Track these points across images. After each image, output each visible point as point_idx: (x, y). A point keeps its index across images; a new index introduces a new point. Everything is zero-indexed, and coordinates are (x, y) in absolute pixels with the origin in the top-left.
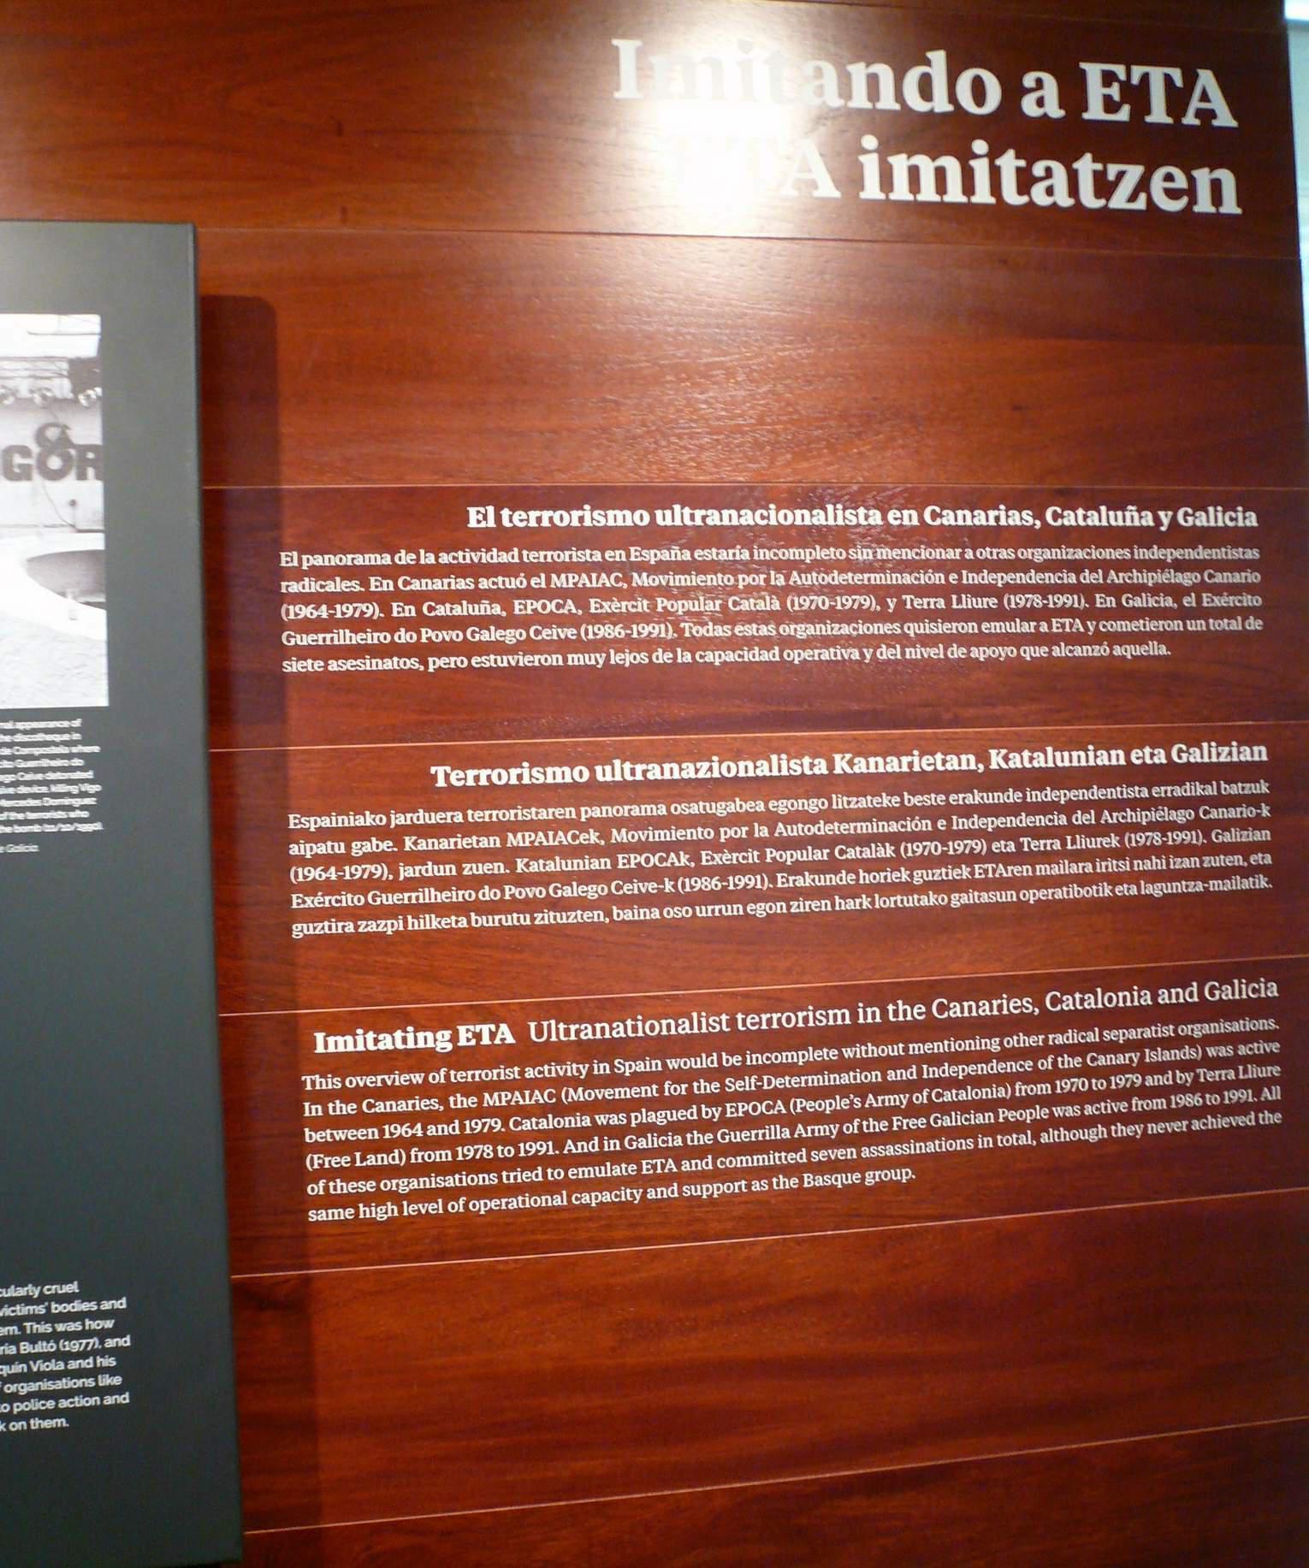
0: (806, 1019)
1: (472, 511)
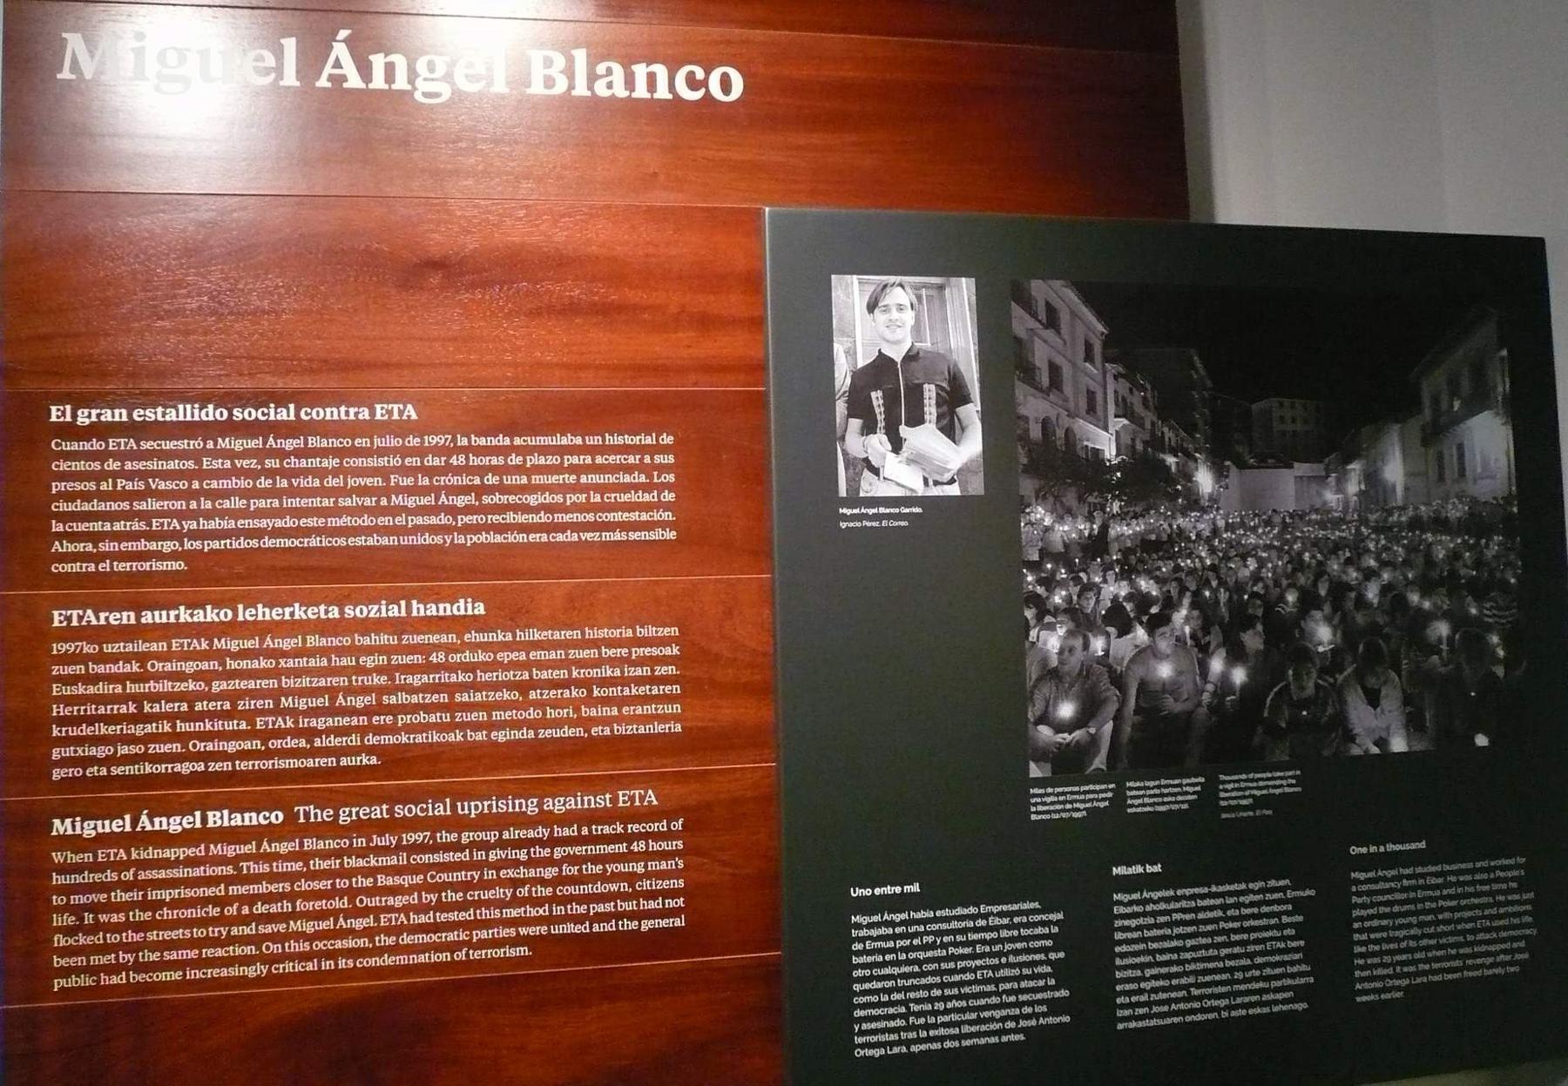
0: (490, 806)
1: (53, 408)
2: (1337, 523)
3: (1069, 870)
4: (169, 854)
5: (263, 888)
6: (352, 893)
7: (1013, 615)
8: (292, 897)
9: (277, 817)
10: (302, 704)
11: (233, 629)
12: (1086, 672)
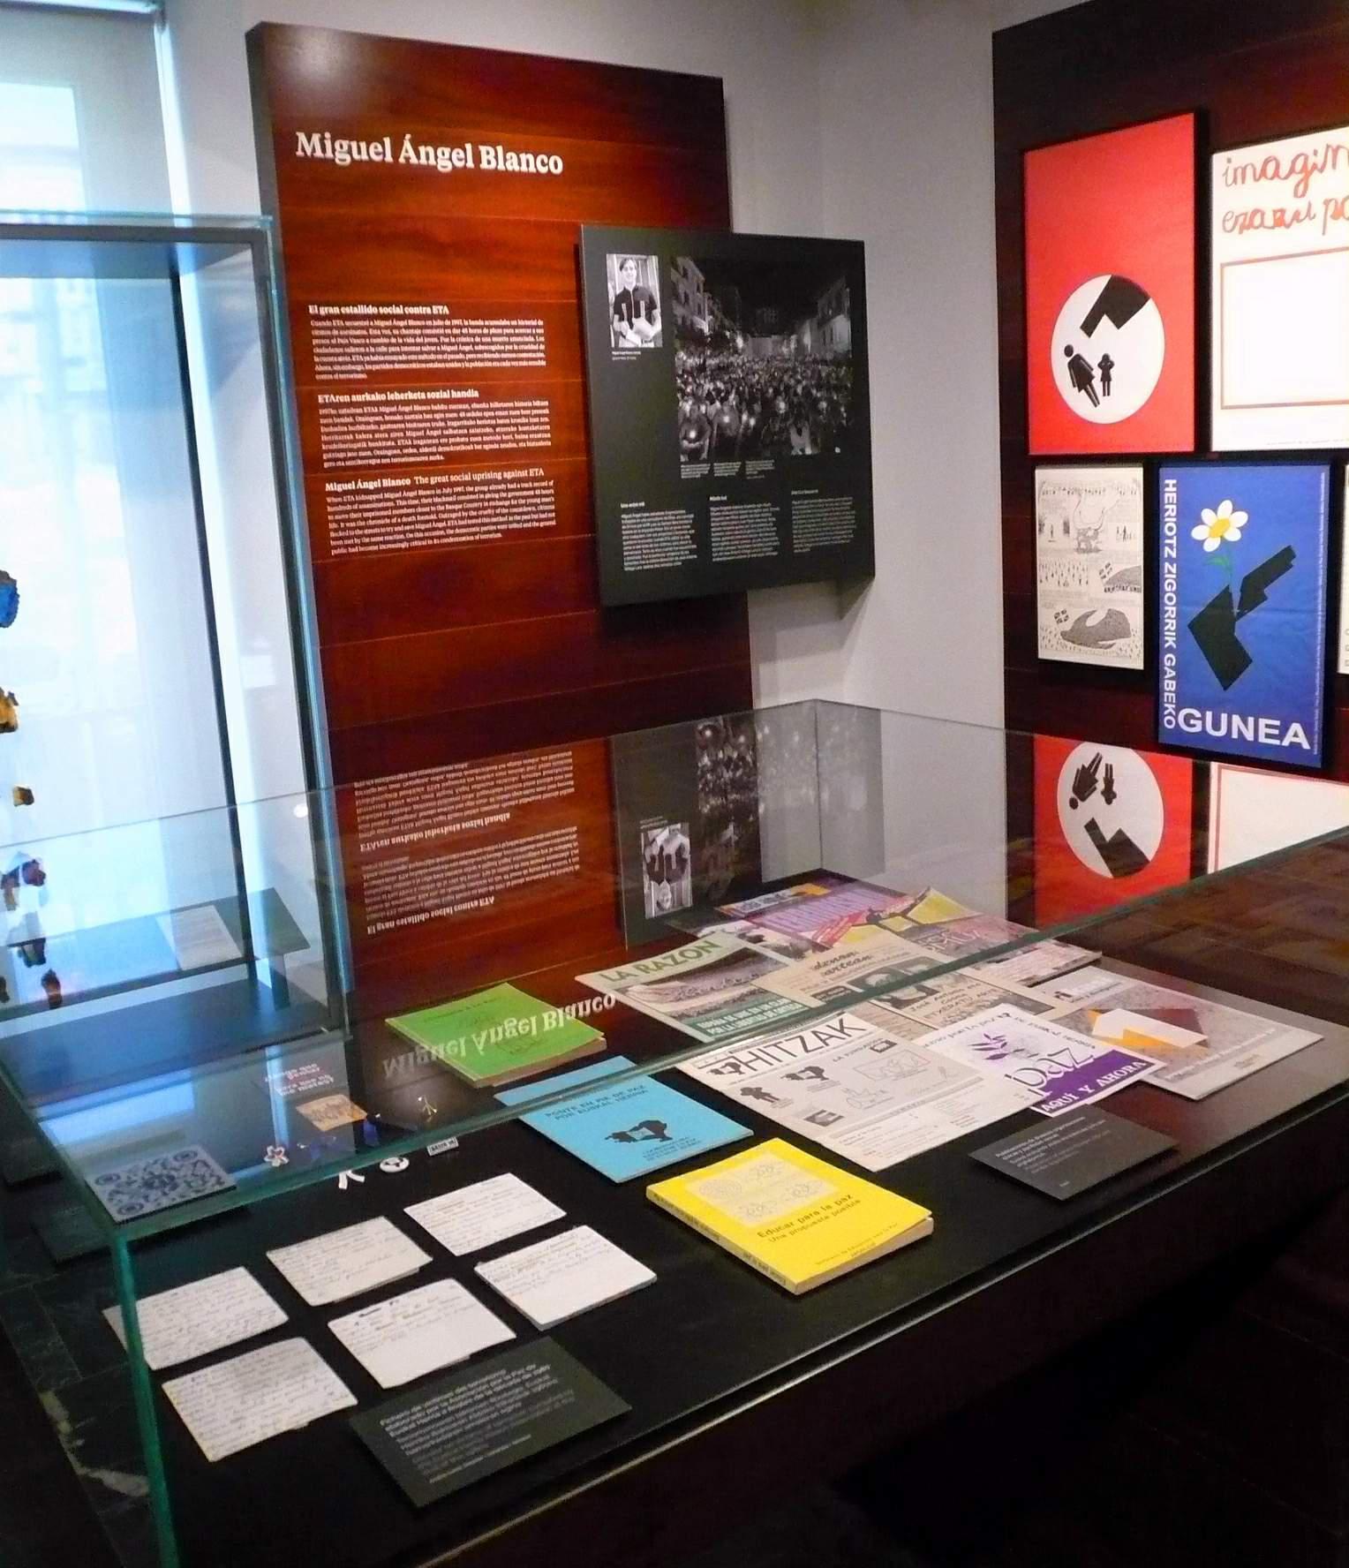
2: (787, 361)
3: (695, 498)
4: (370, 497)
5: (405, 511)
6: (437, 512)
7: (671, 397)
8: (415, 514)
9: (408, 482)
10: (414, 434)
11: (387, 403)
12: (698, 420)
